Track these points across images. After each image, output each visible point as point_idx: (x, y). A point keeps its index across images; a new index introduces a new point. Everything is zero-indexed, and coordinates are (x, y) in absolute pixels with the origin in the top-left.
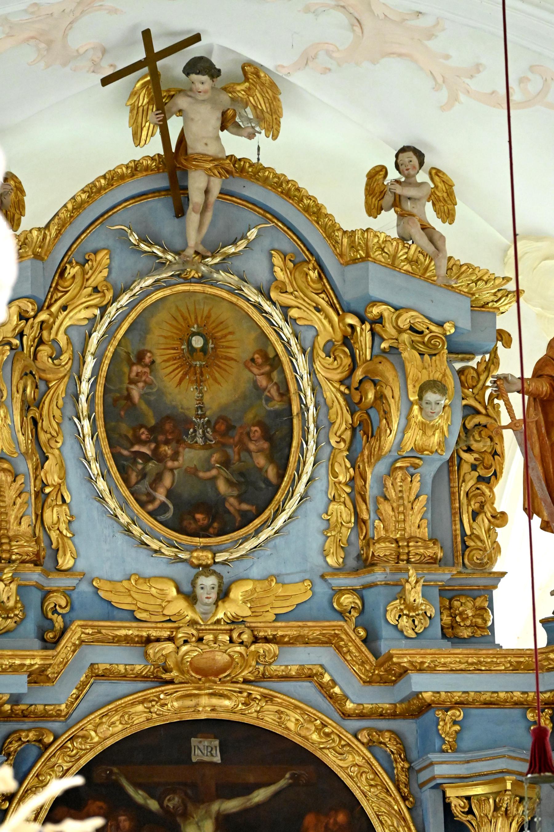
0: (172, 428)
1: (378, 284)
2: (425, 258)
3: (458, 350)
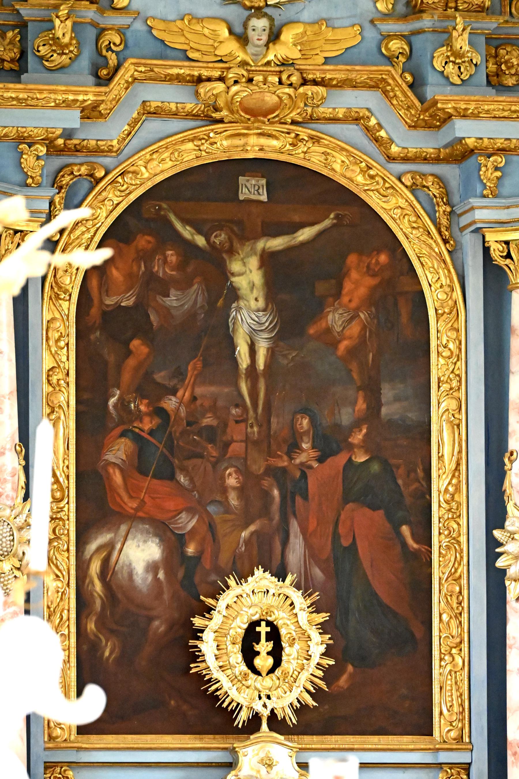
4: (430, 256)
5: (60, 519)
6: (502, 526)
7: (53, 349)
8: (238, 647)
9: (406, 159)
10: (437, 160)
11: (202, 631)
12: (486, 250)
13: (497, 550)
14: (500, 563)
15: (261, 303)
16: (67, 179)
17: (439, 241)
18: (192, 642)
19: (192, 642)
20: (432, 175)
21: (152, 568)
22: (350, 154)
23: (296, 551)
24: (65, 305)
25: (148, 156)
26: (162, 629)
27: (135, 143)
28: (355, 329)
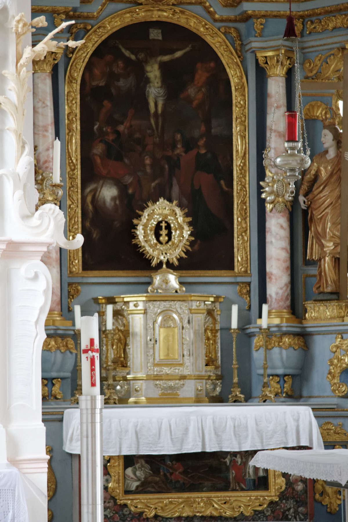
4: (232, 64)
5: (74, 178)
6: (263, 180)
7: (70, 105)
8: (153, 232)
9: (222, 21)
10: (235, 21)
11: (137, 225)
12: (257, 60)
13: (262, 190)
14: (263, 196)
15: (160, 84)
16: (75, 30)
17: (236, 57)
18: (133, 230)
19: (133, 230)
20: (233, 28)
21: (114, 199)
22: (197, 19)
23: (176, 190)
24: (75, 85)
25: (110, 20)
26: (118, 225)
27: (104, 14)
28: (200, 96)
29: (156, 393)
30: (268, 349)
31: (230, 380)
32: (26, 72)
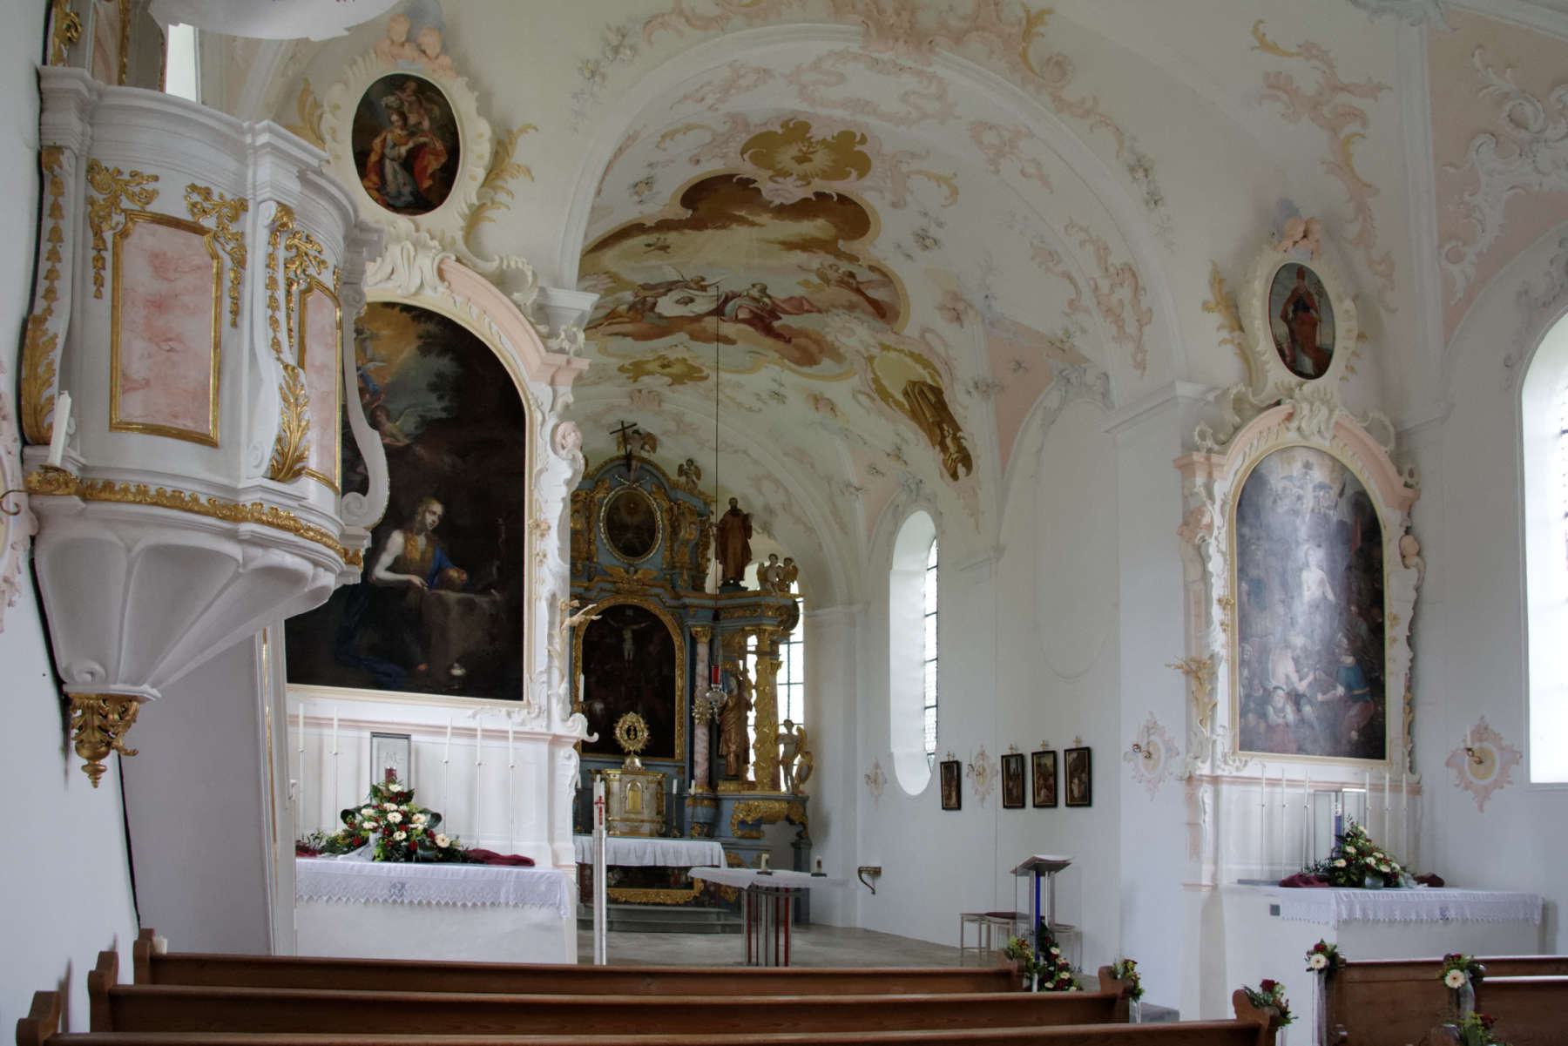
0: (624, 528)
1: (680, 495)
2: (692, 490)
3: (700, 515)
23: (640, 707)
29: (626, 829)
30: (694, 806)
31: (670, 824)
32: (566, 634)
